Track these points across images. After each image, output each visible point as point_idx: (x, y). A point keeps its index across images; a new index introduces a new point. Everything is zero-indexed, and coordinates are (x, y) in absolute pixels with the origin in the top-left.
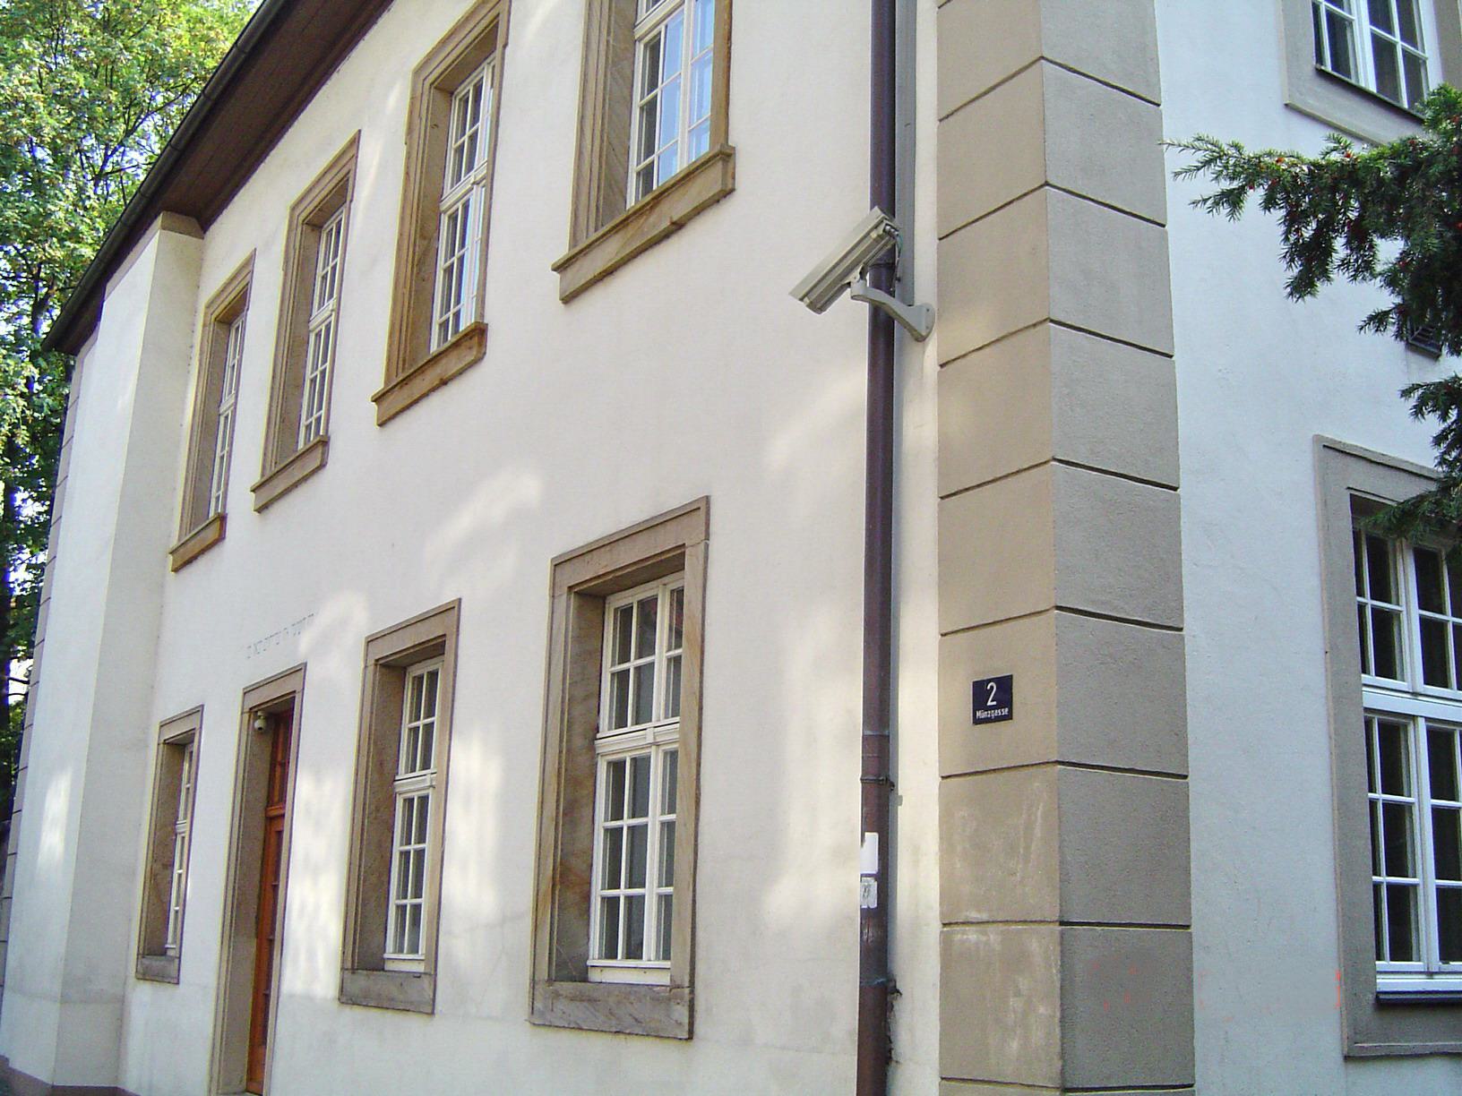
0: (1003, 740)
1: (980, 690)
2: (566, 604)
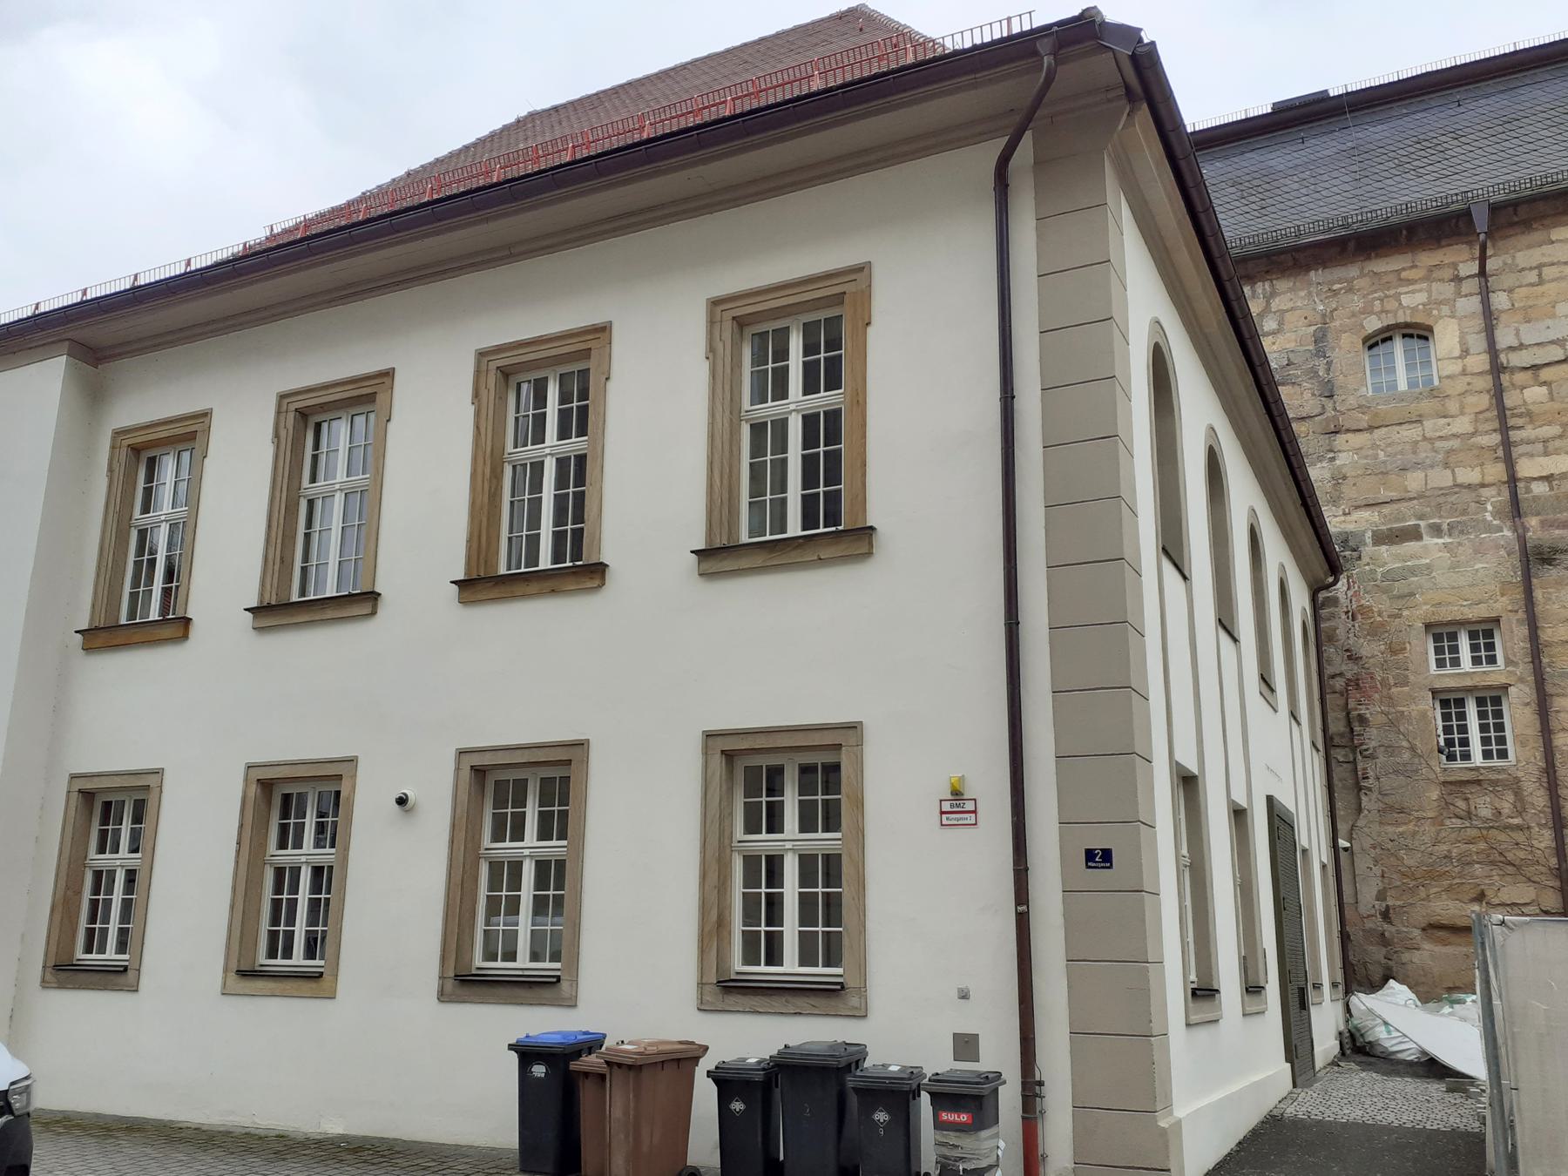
0: (1101, 876)
1: (1090, 855)
2: (466, 773)
